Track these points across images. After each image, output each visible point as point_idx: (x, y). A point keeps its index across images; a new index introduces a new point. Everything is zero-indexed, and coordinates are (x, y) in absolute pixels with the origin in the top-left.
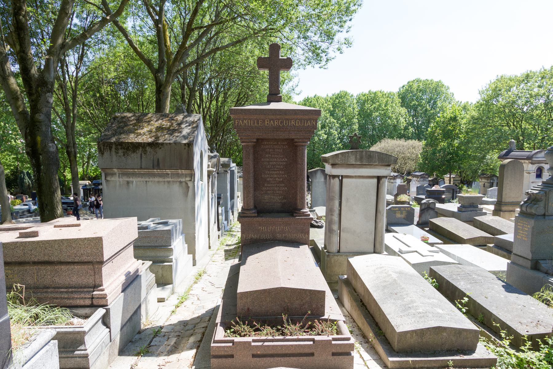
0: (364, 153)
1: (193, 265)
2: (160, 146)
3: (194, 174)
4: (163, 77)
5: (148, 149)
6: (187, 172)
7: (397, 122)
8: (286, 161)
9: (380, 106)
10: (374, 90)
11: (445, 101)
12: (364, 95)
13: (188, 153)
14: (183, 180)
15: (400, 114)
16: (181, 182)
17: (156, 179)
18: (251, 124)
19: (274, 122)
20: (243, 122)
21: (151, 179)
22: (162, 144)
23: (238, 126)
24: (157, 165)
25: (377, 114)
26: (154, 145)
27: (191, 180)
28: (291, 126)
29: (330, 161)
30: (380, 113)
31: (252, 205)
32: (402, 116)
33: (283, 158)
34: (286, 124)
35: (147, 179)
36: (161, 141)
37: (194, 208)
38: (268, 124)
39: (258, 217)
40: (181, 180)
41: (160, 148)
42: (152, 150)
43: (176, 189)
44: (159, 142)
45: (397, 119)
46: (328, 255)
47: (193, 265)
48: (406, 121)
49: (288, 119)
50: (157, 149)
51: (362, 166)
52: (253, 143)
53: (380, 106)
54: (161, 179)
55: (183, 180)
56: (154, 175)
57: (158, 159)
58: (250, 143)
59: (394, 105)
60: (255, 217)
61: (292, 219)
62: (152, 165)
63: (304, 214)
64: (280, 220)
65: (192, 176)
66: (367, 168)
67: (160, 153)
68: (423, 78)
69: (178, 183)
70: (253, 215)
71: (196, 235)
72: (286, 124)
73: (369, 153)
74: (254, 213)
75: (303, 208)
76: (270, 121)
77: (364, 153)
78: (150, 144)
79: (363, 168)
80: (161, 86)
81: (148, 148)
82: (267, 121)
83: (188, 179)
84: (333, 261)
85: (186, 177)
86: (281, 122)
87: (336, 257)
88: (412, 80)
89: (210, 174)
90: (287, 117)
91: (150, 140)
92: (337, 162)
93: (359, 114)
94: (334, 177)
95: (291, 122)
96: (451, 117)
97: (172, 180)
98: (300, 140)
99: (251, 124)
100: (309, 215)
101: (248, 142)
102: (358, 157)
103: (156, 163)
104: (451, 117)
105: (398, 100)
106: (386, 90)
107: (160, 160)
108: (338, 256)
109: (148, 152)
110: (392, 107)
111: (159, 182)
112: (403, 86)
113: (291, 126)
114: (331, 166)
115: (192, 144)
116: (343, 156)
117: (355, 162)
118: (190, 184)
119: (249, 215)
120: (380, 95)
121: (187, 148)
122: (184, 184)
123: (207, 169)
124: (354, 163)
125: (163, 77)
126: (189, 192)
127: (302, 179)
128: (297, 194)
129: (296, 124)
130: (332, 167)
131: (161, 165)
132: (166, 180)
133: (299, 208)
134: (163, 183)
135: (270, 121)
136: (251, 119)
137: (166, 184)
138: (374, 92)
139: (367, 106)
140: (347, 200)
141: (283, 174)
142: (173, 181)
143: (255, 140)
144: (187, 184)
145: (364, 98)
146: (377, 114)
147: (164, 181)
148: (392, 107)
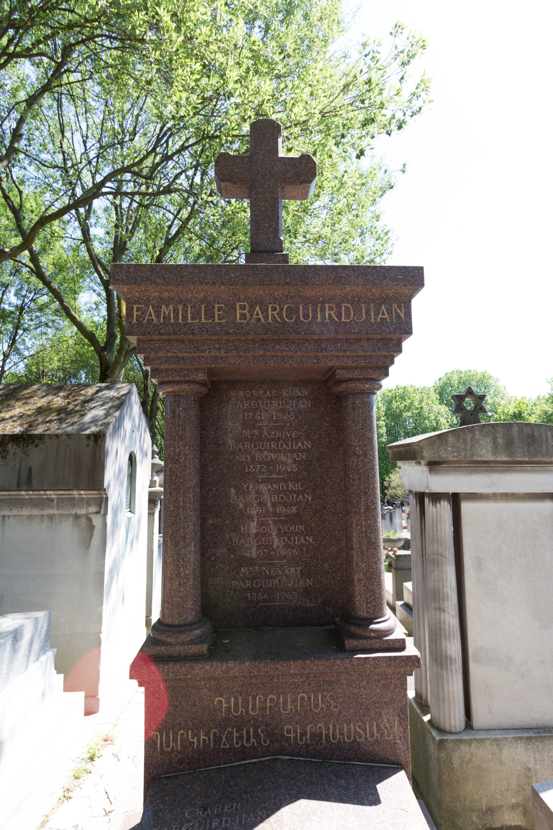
0: (516, 429)
1: (88, 713)
2: (37, 441)
3: (107, 499)
4: (112, 357)
5: (11, 448)
6: (92, 494)
7: (437, 423)
8: (307, 450)
9: (412, 403)
10: (402, 384)
11: (495, 395)
12: (390, 391)
13: (94, 453)
14: (83, 511)
15: (439, 413)
16: (77, 517)
17: (25, 512)
18: (185, 318)
19: (265, 311)
20: (157, 311)
21: (15, 512)
22: (41, 437)
23: (140, 324)
24: (26, 481)
25: (409, 414)
26: (22, 439)
27: (98, 513)
28: (323, 324)
29: (425, 454)
30: (412, 413)
31: (190, 611)
32: (442, 416)
33: (297, 439)
34: (306, 316)
35: (6, 512)
36: (40, 430)
37: (103, 573)
38: (243, 316)
39: (212, 655)
40: (79, 512)
41: (37, 446)
42: (18, 450)
43: (67, 531)
44: (36, 432)
45: (435, 419)
46: (441, 742)
47: (88, 713)
48: (448, 422)
49: (312, 301)
50: (30, 447)
51: (511, 466)
52: (195, 387)
53: (412, 403)
54: (35, 512)
55: (83, 511)
56: (21, 503)
57: (30, 469)
58: (185, 387)
59: (430, 402)
60: (196, 658)
61: (339, 663)
62: (15, 481)
63: (382, 642)
64: (294, 667)
65: (102, 502)
66: (524, 471)
67: (35, 456)
68: (463, 369)
69: (71, 519)
70: (194, 649)
71: (102, 636)
72: (306, 316)
73: (528, 430)
74: (200, 640)
75: (376, 614)
76: (252, 307)
77: (516, 429)
78: (14, 438)
79: (513, 471)
80: (107, 368)
81: (10, 446)
82: (243, 308)
83: (92, 509)
84: (456, 763)
85: (89, 505)
86: (292, 311)
87: (464, 748)
88: (451, 371)
89: (152, 500)
90: (308, 292)
91: (18, 430)
92: (444, 455)
93: (385, 415)
94: (436, 497)
95: (323, 310)
96: (514, 413)
97: (60, 512)
98: (356, 374)
99: (185, 318)
100: (400, 645)
101: (179, 383)
102: (500, 440)
103: (24, 477)
104: (514, 413)
105: (435, 396)
106: (419, 384)
107: (34, 472)
108: (469, 743)
109: (11, 454)
110: (427, 404)
111: (30, 517)
112: (440, 379)
113: (323, 324)
114: (425, 469)
115: (105, 436)
116: (458, 439)
117: (494, 454)
118: (96, 521)
119: (178, 649)
120: (411, 390)
121: (91, 443)
122: (83, 520)
123: (147, 490)
124: (490, 458)
125: (112, 357)
126: (92, 536)
127: (368, 509)
128: (349, 561)
129: (339, 315)
130: (431, 471)
131: (35, 481)
132: (46, 512)
133: (362, 613)
134: (38, 520)
135: (252, 307)
136: (185, 303)
137: (46, 520)
138: (403, 386)
139: (394, 405)
140: (479, 564)
141: (298, 493)
142: (61, 515)
143: (201, 377)
144: (89, 520)
145: (390, 394)
146: (409, 414)
147: (42, 516)
148: (427, 404)
